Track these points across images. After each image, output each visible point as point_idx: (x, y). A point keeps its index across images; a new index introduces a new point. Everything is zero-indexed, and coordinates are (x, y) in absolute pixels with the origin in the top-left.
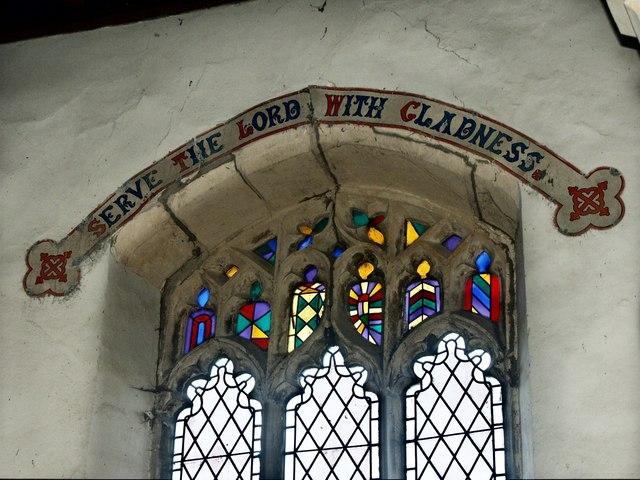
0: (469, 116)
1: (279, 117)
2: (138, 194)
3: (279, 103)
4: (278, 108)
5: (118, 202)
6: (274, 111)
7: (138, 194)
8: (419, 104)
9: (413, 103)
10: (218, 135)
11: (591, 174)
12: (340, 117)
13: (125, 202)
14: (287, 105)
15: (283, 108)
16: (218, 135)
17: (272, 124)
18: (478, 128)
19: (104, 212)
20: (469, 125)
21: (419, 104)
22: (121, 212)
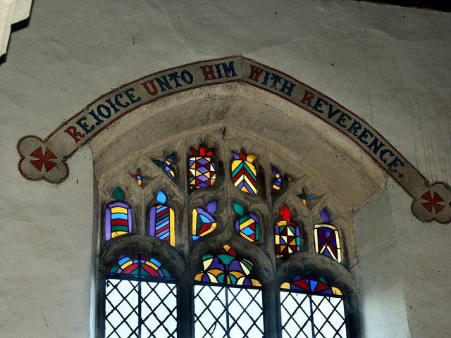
0: (66, 127)
1: (356, 132)
2: (331, 115)
3: (364, 126)
4: (360, 127)
5: (355, 122)
6: (309, 96)
7: (331, 115)
8: (394, 155)
9: (391, 152)
10: (402, 165)
11: (66, 165)
12: (160, 93)
13: (357, 128)
14: (355, 122)
15: (362, 130)
16: (402, 165)
17: (382, 145)
18: (379, 153)
19: (345, 115)
20: (72, 130)
21: (394, 155)
22: (369, 144)
